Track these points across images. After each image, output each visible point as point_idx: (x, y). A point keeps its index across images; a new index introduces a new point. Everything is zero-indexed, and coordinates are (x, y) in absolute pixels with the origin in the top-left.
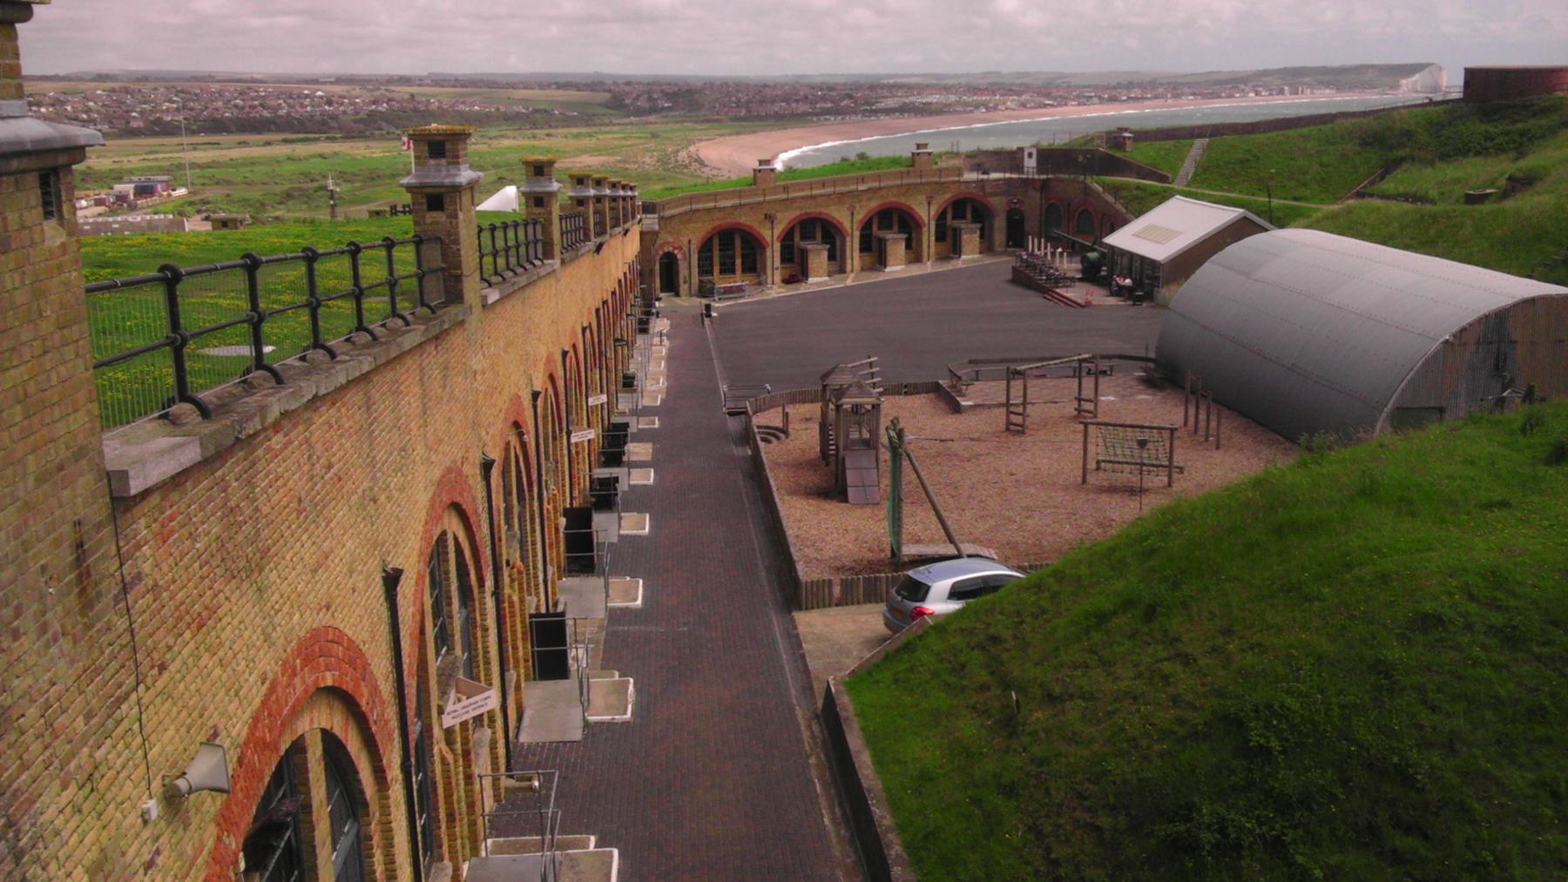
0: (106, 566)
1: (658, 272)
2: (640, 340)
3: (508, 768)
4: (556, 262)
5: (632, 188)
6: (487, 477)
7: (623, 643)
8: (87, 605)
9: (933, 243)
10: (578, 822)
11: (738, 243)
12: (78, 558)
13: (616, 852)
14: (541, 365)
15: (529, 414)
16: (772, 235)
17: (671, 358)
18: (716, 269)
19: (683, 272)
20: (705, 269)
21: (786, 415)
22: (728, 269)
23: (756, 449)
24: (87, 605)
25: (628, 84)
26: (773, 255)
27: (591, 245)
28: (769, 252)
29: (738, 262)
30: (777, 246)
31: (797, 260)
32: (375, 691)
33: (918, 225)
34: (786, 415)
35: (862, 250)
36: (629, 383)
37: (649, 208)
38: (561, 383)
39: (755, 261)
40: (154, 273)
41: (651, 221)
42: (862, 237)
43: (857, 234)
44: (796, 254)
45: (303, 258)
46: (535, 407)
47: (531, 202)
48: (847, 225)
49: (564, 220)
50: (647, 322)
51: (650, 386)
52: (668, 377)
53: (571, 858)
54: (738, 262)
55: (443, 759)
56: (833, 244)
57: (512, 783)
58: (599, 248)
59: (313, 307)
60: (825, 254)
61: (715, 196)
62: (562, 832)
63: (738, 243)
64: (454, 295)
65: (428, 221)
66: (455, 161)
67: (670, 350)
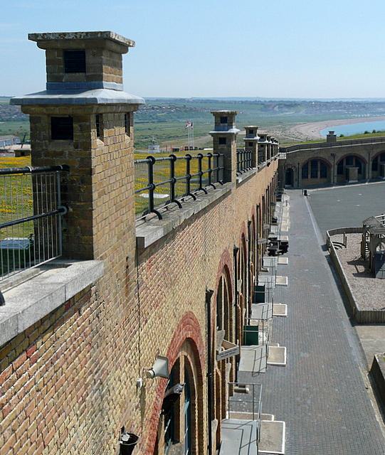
0: (134, 277)
1: (286, 179)
2: (278, 204)
3: (236, 381)
4: (256, 169)
5: (277, 142)
6: (235, 255)
7: (282, 330)
8: (127, 293)
9: (370, 172)
10: (269, 408)
11: (319, 165)
12: (126, 272)
13: (284, 423)
14: (251, 211)
15: (247, 230)
16: (334, 163)
17: (291, 212)
18: (309, 176)
19: (295, 177)
20: (304, 176)
21: (345, 239)
22: (314, 176)
23: (332, 252)
24: (127, 293)
25: (271, 101)
26: (334, 171)
27: (265, 163)
28: (332, 169)
29: (319, 173)
30: (336, 167)
31: (345, 173)
32: (202, 342)
33: (365, 162)
34: (345, 239)
35: (373, 169)
36: (274, 221)
37: (282, 150)
38: (256, 219)
39: (326, 173)
40: (196, 156)
41: (283, 156)
42: (373, 164)
43: (371, 163)
44: (344, 171)
45: (148, 162)
46: (249, 227)
47: (248, 144)
48: (367, 159)
49: (255, 151)
50: (280, 196)
51: (284, 223)
52: (290, 219)
53: (265, 424)
54: (319, 173)
55: (217, 374)
56: (361, 167)
57: (237, 388)
58: (268, 164)
59: (173, 184)
60: (357, 171)
61: (310, 146)
62: (263, 413)
63: (319, 165)
64: (227, 179)
65: (219, 148)
66: (231, 127)
67: (290, 208)
